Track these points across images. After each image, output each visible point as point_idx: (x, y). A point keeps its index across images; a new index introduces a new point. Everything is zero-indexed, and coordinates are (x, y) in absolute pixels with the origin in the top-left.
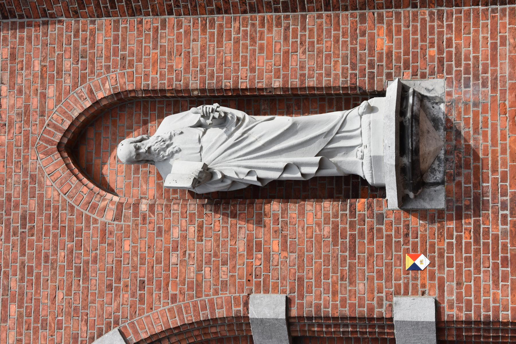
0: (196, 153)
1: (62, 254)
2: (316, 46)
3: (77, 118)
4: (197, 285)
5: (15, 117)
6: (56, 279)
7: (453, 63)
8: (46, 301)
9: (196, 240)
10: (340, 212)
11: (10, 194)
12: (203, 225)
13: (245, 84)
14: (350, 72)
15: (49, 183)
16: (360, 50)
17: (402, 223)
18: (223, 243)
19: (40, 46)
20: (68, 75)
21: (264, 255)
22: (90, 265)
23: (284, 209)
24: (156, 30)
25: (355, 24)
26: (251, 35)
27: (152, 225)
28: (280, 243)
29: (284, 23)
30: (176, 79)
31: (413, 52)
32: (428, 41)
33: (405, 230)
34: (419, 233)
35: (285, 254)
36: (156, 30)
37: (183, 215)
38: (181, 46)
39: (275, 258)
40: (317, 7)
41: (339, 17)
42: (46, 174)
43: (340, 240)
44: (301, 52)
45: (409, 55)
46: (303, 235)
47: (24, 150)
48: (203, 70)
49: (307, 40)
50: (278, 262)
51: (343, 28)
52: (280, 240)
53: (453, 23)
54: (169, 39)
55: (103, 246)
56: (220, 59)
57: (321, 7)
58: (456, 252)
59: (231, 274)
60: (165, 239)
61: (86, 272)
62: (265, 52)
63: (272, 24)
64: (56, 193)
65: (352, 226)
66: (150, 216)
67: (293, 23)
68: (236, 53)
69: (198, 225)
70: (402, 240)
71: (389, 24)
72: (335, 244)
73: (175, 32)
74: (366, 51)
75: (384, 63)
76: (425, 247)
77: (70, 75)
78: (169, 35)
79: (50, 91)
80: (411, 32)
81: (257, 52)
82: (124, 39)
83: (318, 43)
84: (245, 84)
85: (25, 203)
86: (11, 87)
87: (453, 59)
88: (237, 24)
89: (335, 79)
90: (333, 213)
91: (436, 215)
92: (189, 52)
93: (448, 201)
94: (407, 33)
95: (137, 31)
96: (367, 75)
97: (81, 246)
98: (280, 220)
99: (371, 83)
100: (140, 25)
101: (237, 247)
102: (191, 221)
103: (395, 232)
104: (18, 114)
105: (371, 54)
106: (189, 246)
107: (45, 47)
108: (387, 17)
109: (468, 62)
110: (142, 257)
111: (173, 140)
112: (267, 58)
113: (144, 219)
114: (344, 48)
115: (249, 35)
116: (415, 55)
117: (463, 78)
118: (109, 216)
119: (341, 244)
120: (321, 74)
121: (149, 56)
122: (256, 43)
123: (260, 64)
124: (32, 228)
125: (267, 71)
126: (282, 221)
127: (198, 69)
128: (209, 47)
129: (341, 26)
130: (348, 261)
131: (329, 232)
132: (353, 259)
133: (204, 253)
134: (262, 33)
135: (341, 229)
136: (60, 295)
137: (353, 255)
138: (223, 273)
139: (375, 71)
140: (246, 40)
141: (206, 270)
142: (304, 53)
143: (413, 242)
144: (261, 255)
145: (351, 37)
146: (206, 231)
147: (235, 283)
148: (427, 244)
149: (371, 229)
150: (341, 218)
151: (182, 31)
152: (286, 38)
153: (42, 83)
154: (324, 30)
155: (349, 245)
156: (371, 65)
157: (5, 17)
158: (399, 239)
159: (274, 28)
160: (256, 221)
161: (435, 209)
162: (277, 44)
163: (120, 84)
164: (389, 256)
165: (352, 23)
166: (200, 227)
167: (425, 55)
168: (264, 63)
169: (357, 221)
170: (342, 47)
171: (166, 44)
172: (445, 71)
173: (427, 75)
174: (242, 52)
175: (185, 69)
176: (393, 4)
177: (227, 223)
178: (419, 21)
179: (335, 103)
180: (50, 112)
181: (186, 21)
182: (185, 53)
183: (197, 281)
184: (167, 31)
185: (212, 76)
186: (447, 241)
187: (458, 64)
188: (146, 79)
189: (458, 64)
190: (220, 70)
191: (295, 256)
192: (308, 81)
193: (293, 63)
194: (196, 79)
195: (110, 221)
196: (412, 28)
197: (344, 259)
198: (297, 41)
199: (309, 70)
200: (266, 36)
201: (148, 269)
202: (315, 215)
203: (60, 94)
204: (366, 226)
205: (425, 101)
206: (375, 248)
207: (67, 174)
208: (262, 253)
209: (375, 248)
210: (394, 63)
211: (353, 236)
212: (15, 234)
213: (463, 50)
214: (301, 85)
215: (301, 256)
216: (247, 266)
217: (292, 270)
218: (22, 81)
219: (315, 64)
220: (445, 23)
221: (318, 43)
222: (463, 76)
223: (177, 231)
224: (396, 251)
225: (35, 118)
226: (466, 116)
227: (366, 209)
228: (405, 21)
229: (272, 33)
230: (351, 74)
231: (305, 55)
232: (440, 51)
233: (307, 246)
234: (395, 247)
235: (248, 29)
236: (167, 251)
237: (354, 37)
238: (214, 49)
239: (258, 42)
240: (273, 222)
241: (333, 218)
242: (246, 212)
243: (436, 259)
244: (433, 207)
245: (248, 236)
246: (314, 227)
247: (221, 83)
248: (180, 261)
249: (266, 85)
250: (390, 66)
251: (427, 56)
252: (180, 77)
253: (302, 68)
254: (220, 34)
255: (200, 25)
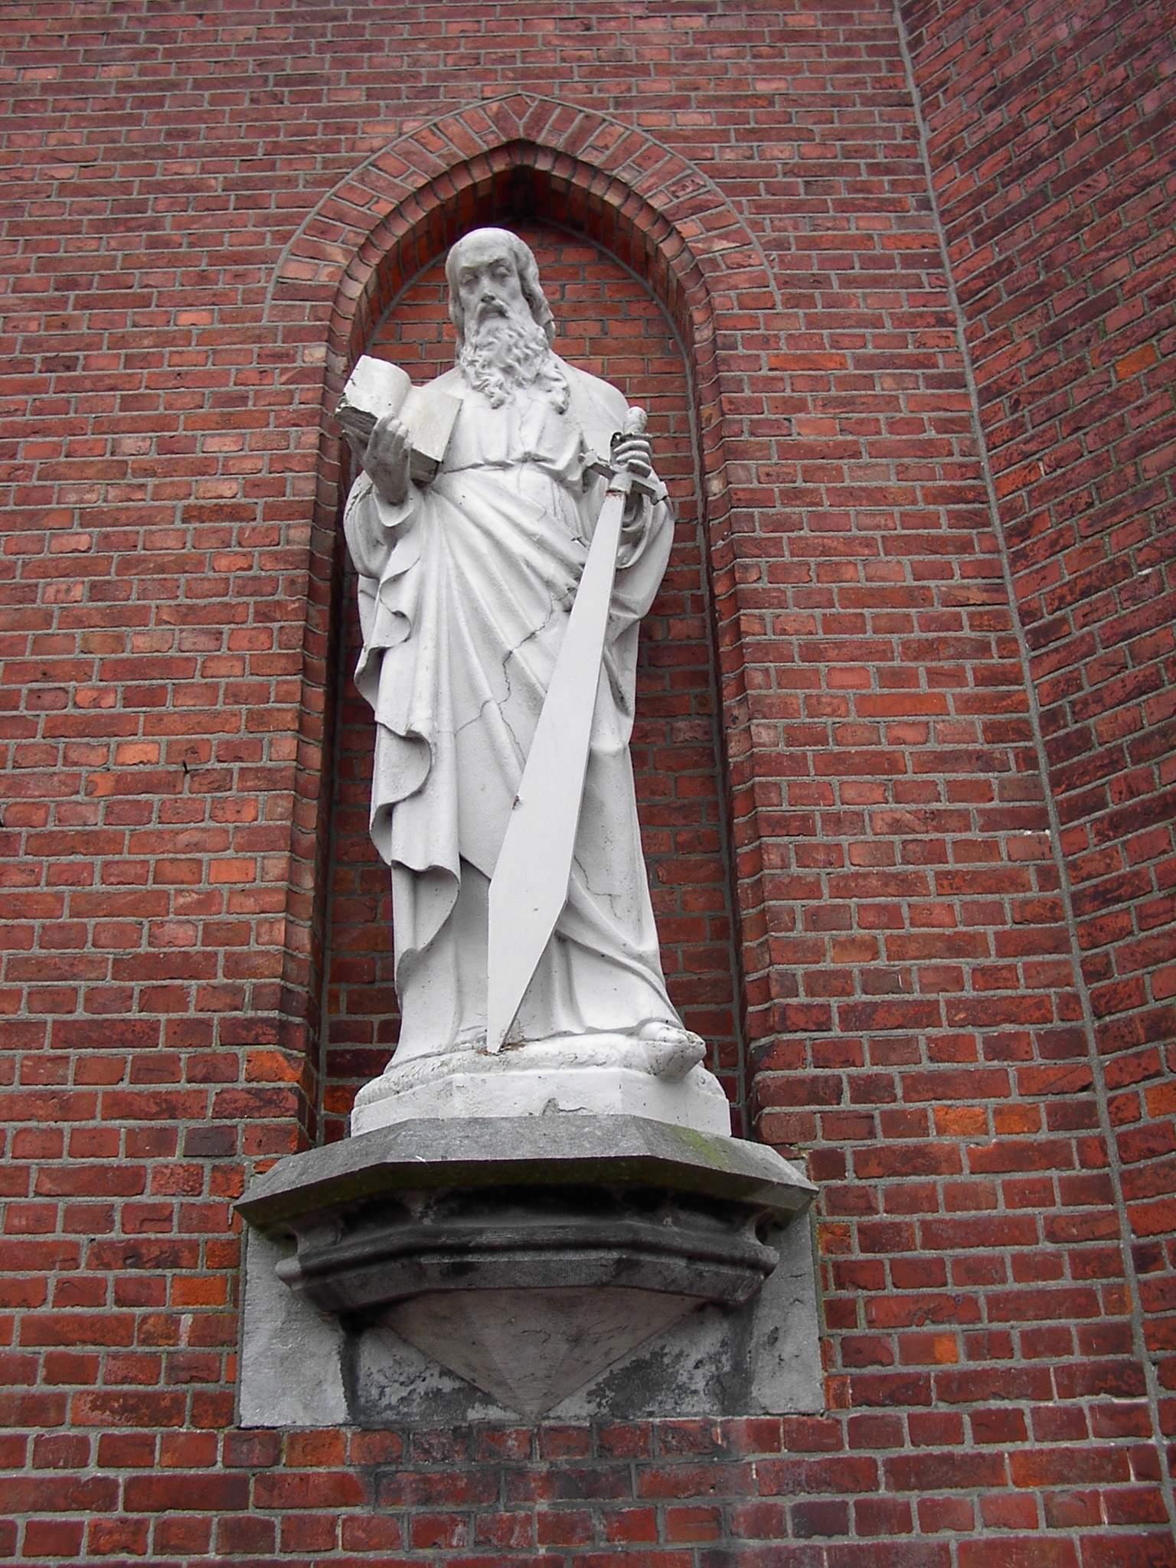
0: (480, 449)
1: (190, 170)
2: (929, 870)
3: (613, 182)
4: (33, 514)
5: (611, 46)
6: (114, 160)
7: (908, 1450)
8: (53, 141)
9: (192, 501)
10: (248, 984)
11: (380, 49)
12: (241, 520)
13: (757, 628)
14: (834, 1002)
15: (410, 126)
16: (929, 1039)
17: (186, 1236)
18: (169, 585)
19: (830, 90)
20: (747, 154)
21: (112, 716)
22: (145, 234)
23: (278, 776)
24: (927, 362)
25: (1037, 1014)
26: (943, 641)
27: (254, 377)
28: (148, 768)
29: (1008, 749)
30: (758, 421)
31: (940, 1261)
32: (996, 1326)
33: (155, 1251)
34: (138, 1311)
35: (105, 785)
36: (927, 362)
37: (283, 463)
38: (879, 433)
39: (92, 754)
40: (1085, 860)
41: (1055, 950)
42: (437, 119)
43: (137, 985)
44: (898, 816)
45: (923, 1247)
46: (170, 846)
47: (514, 70)
48: (797, 498)
49: (949, 837)
50: (75, 764)
51: (1012, 968)
52: (159, 768)
53: (1093, 1442)
54: (897, 398)
55: (200, 260)
56: (841, 547)
57: (1089, 877)
58: (42, 1481)
59: (56, 614)
60: (204, 418)
61: (127, 226)
62: (885, 691)
63: (995, 710)
64: (377, 143)
65: (193, 1032)
66: (284, 371)
67: (1010, 781)
68: (872, 596)
69: (240, 505)
70: (115, 1235)
71: (1053, 1155)
72: (121, 968)
73: (925, 416)
74: (927, 1066)
75: (881, 1141)
76: (75, 1336)
77: (751, 158)
78: (909, 397)
79: (696, 116)
80: (1026, 1249)
81: (882, 664)
82: (876, 282)
83: (938, 875)
84: (757, 628)
85: (352, 80)
86: (700, 37)
87: (924, 1450)
88: (977, 596)
89: (796, 945)
90: (248, 955)
91: (210, 1387)
92: (857, 455)
93: (270, 1435)
94: (1022, 1232)
95: (911, 314)
96: (828, 1072)
97: (208, 209)
98: (236, 766)
99: (792, 1092)
100: (932, 321)
101: (151, 626)
102: (253, 487)
103: (153, 1207)
104: (621, 52)
105: (916, 1086)
106: (172, 483)
107: (829, 102)
108: (1081, 1143)
109: (916, 1523)
110: (149, 358)
111: (533, 391)
112: (862, 700)
113: (278, 357)
114: (930, 977)
115: (942, 634)
116: (931, 1274)
117: (839, 1498)
118: (298, 271)
119: (122, 989)
120: (814, 891)
121: (832, 347)
122: (916, 659)
123: (837, 676)
124: (277, 99)
125: (814, 701)
126: (230, 771)
127: (800, 483)
128: (882, 513)
129: (1019, 962)
130: (50, 1017)
131: (169, 944)
132: (55, 1035)
133: (142, 529)
134: (956, 677)
135: (182, 987)
136: (65, 172)
137: (69, 1035)
138: (64, 587)
139: (846, 1105)
140: (925, 628)
141: (82, 539)
142: (896, 826)
143: (101, 1283)
144: (113, 705)
145: (979, 1001)
146: (217, 531)
147: (22, 628)
148: (90, 1348)
149: (170, 1107)
150: (225, 987)
151: (932, 434)
152: (941, 761)
153: (719, 100)
154: (996, 897)
155: (113, 1022)
156: (869, 1089)
157: (906, 13)
158: (118, 1226)
159: (978, 720)
160: (238, 685)
161: (234, 1381)
162: (922, 730)
163: (729, 276)
164: (52, 1180)
165: (1040, 1003)
166: (236, 513)
167: (935, 1314)
168: (842, 687)
169: (208, 1050)
170: (936, 968)
171: (878, 391)
172: (864, 1410)
173: (844, 1332)
174: (876, 617)
175: (798, 446)
176: (1141, 1164)
177: (239, 594)
178: (1080, 1283)
179: (709, 975)
180: (628, 118)
181: (968, 442)
182: (856, 442)
183: (49, 512)
184: (923, 390)
185: (781, 524)
186: (94, 1436)
187: (903, 1473)
188: (748, 342)
189: (903, 1473)
190: (801, 548)
191: (92, 820)
192: (786, 846)
193: (849, 791)
194: (763, 478)
195: (276, 273)
196: (1045, 1254)
197: (61, 1001)
198: (938, 800)
199: (828, 847)
200: (950, 692)
201: (109, 376)
202: (243, 886)
203: (686, 139)
204: (183, 1086)
205: (726, 1325)
206: (91, 1124)
207: (436, 165)
208: (120, 709)
209: (91, 1124)
210: (882, 1181)
211: (145, 1034)
212: (261, 65)
213: (970, 1496)
214: (769, 820)
215: (90, 842)
216: (77, 664)
217: (42, 813)
218: (720, 57)
219: (853, 869)
220: (1084, 1402)
221: (938, 875)
222: (851, 1499)
223: (226, 449)
224: (70, 1212)
225: (612, 88)
226: (660, 1520)
227: (254, 1085)
228: (1072, 1220)
229: (959, 711)
230: (826, 1008)
231: (885, 829)
232: (957, 1387)
233: (127, 862)
234: (89, 1209)
235: (967, 632)
236: (162, 424)
237: (980, 1014)
238: (878, 527)
239: (921, 667)
240: (228, 742)
241: (228, 956)
242: (275, 650)
243: (20, 1388)
244: (246, 1374)
245: (188, 659)
246: (196, 887)
247: (756, 552)
248: (126, 462)
249: (758, 699)
250: (874, 1168)
251: (929, 1328)
252: (766, 431)
253: (835, 822)
254: (936, 545)
255: (957, 483)
